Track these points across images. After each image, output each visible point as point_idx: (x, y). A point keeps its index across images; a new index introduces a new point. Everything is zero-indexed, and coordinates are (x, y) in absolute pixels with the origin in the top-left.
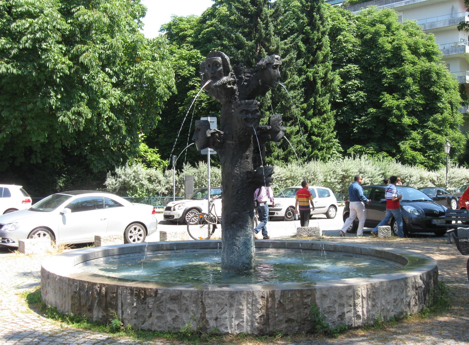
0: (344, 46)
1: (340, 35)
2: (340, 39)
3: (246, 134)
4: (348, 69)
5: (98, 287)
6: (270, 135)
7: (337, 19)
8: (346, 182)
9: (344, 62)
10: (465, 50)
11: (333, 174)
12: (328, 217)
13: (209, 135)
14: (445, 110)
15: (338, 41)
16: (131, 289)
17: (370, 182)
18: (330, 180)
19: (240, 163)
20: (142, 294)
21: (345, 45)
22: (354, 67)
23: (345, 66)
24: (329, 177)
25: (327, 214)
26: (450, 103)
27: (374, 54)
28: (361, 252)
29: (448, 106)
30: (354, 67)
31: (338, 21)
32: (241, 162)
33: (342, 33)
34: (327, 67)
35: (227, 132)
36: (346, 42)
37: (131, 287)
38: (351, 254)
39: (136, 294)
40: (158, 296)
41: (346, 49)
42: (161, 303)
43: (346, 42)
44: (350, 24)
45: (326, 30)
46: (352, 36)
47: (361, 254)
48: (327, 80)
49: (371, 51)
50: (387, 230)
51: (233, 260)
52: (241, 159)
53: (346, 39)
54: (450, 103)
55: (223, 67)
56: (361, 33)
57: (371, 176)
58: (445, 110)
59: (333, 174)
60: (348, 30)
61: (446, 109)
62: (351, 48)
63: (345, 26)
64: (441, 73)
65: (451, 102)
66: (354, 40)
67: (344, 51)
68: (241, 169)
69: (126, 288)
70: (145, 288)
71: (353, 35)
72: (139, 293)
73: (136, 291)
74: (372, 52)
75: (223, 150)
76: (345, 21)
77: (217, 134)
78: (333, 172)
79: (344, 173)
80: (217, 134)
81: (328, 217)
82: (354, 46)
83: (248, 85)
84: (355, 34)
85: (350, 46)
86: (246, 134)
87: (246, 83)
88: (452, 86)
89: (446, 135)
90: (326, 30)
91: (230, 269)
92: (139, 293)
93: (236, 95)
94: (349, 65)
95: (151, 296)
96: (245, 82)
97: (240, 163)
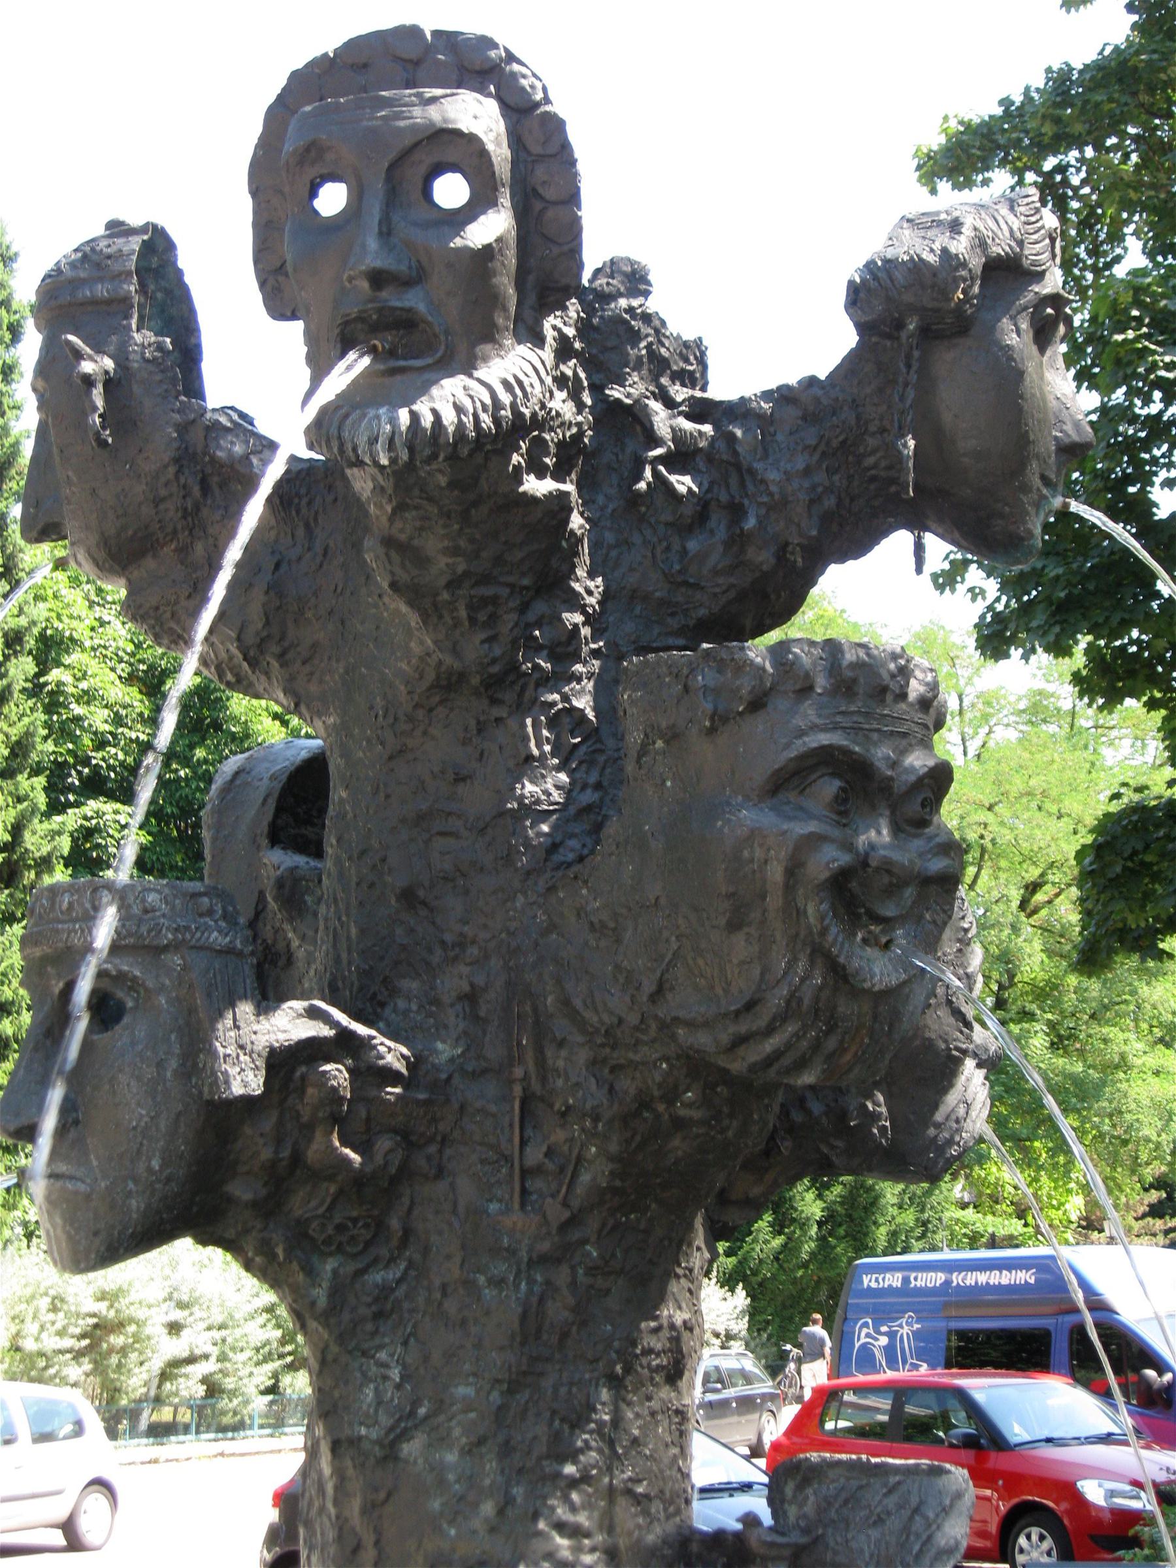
0: (78, 719)
1: (59, 664)
2: (59, 684)
3: (808, 1078)
4: (86, 818)
6: (878, 1104)
7: (50, 593)
8: (111, 1351)
9: (71, 788)
11: (54, 1309)
12: (74, 1544)
15: (52, 693)
17: (215, 1351)
18: (37, 1339)
19: (609, 1437)
21: (78, 710)
22: (116, 812)
23: (77, 805)
24: (32, 1328)
25: (68, 1527)
27: (206, 761)
30: (116, 812)
31: (51, 604)
32: (616, 1422)
33: (67, 660)
34: (20, 800)
35: (445, 1051)
36: (87, 697)
41: (82, 728)
43: (87, 697)
44: (102, 623)
45: (28, 629)
46: (113, 676)
48: (22, 857)
49: (192, 747)
52: (616, 1383)
53: (84, 685)
55: (522, 215)
56: (152, 667)
57: (218, 1318)
59: (54, 1309)
60: (93, 649)
62: (107, 728)
63: (81, 631)
66: (118, 692)
67: (75, 739)
68: (627, 1516)
71: (113, 669)
74: (200, 753)
75: (377, 1277)
76: (81, 608)
77: (337, 1073)
78: (54, 1298)
79: (102, 1307)
80: (337, 1073)
81: (74, 1544)
82: (118, 721)
83: (702, 506)
84: (123, 669)
85: (99, 719)
86: (808, 1078)
87: (683, 483)
90: (28, 629)
93: (574, 602)
94: (91, 803)
97: (609, 1437)
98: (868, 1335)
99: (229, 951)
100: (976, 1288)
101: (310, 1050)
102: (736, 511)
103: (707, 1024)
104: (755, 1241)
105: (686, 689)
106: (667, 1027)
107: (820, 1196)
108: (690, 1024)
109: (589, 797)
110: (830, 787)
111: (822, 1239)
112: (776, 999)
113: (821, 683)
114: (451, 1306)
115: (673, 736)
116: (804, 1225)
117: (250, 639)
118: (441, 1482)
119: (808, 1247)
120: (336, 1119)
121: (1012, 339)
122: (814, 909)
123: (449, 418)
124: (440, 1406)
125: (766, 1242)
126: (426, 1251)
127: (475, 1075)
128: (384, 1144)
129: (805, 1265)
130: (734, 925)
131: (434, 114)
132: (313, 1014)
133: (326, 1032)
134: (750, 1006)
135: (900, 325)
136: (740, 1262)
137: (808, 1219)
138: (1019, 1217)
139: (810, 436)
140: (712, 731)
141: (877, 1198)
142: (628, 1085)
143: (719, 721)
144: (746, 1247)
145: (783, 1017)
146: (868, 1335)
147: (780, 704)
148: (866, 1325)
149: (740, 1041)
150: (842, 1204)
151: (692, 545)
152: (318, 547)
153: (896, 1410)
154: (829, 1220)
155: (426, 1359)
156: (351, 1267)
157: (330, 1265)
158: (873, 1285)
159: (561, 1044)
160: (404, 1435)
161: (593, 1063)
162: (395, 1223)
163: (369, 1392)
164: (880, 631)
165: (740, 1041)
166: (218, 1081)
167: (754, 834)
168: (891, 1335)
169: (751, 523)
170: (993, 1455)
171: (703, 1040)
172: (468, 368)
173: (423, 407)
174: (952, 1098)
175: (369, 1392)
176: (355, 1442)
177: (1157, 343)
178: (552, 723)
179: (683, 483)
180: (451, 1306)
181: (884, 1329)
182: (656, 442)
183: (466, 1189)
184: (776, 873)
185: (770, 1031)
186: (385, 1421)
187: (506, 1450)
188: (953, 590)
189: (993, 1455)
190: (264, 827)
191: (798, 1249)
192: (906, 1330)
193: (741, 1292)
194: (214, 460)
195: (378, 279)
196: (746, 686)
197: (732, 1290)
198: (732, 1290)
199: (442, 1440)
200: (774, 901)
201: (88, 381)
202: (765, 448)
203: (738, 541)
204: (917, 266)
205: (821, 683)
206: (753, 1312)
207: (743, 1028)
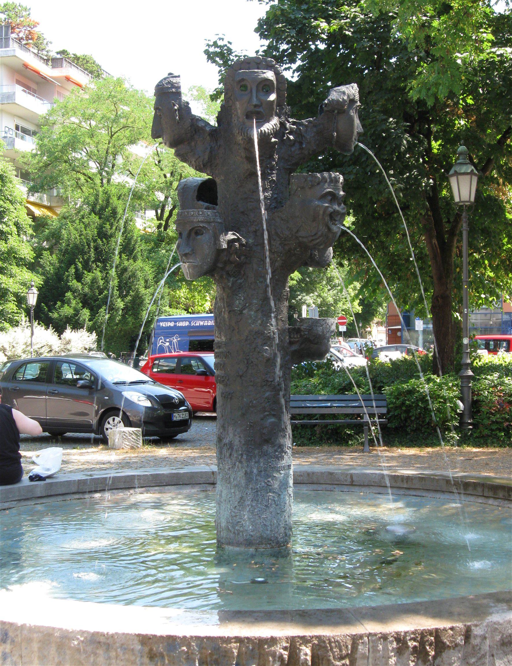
5: (285, 649)
10: (14, 145)
13: (225, 246)
14: (10, 236)
16: (400, 639)
20: (430, 645)
26: (17, 224)
28: (352, 481)
29: (14, 229)
35: (251, 241)
37: (397, 633)
38: (329, 487)
39: (415, 647)
40: (475, 642)
42: (480, 658)
47: (352, 484)
50: (136, 435)
51: (268, 523)
54: (17, 224)
58: (10, 236)
61: (11, 234)
64: (6, 177)
65: (18, 223)
69: (384, 637)
70: (437, 630)
72: (422, 643)
73: (414, 639)
75: (239, 281)
83: (294, 141)
87: (292, 137)
88: (19, 199)
89: (11, 276)
91: (261, 543)
92: (422, 643)
93: (274, 160)
95: (457, 645)
96: (290, 133)
98: (162, 342)
99: (221, 223)
100: (200, 327)
101: (233, 241)
102: (301, 143)
103: (306, 237)
104: (99, 316)
105: (306, 180)
106: (297, 238)
107: (123, 300)
108: (303, 237)
109: (275, 196)
110: (330, 198)
111: (123, 316)
112: (320, 233)
113: (328, 180)
114: (252, 287)
115: (302, 188)
116: (117, 310)
117: (205, 162)
118: (251, 317)
119: (118, 318)
120: (236, 253)
121: (352, 114)
122: (327, 218)
123: (267, 131)
124: (251, 304)
125: (103, 316)
126: (247, 277)
127: (257, 245)
128: (243, 258)
129: (117, 325)
130: (314, 221)
131: (265, 76)
132: (234, 234)
133: (236, 237)
134: (315, 234)
135: (334, 111)
136: (94, 323)
137: (118, 308)
138: (185, 310)
139: (315, 130)
140: (310, 188)
141: (143, 301)
142: (287, 248)
143: (312, 186)
144: (96, 318)
145: (320, 237)
146: (162, 342)
147: (322, 184)
148: (161, 339)
149: (313, 240)
150: (130, 303)
151: (293, 149)
152: (218, 144)
153: (178, 363)
154: (126, 309)
155: (248, 296)
156: (235, 279)
157: (232, 279)
158: (164, 326)
159: (275, 240)
160: (244, 309)
161: (280, 244)
162: (242, 272)
163: (238, 302)
164: (146, 93)
165: (313, 240)
166: (220, 245)
167: (318, 206)
168: (170, 342)
169: (304, 146)
170: (211, 377)
171: (305, 240)
172: (268, 122)
173: (262, 129)
174: (327, 252)
175: (238, 302)
176: (234, 311)
177: (288, 29)
178: (270, 182)
179: (292, 137)
180: (252, 287)
181: (168, 340)
182: (287, 129)
183: (255, 266)
184: (321, 212)
185: (318, 238)
186: (241, 307)
187: (263, 311)
188: (216, 101)
189: (211, 377)
190: (195, 197)
191: (115, 319)
192: (175, 340)
193: (94, 334)
194: (198, 126)
195: (255, 106)
196: (317, 181)
197: (91, 333)
198: (91, 333)
199: (251, 310)
200: (320, 217)
201: (176, 110)
202: (306, 131)
203: (301, 149)
204: (338, 101)
205: (328, 180)
206: (99, 341)
207: (314, 238)
